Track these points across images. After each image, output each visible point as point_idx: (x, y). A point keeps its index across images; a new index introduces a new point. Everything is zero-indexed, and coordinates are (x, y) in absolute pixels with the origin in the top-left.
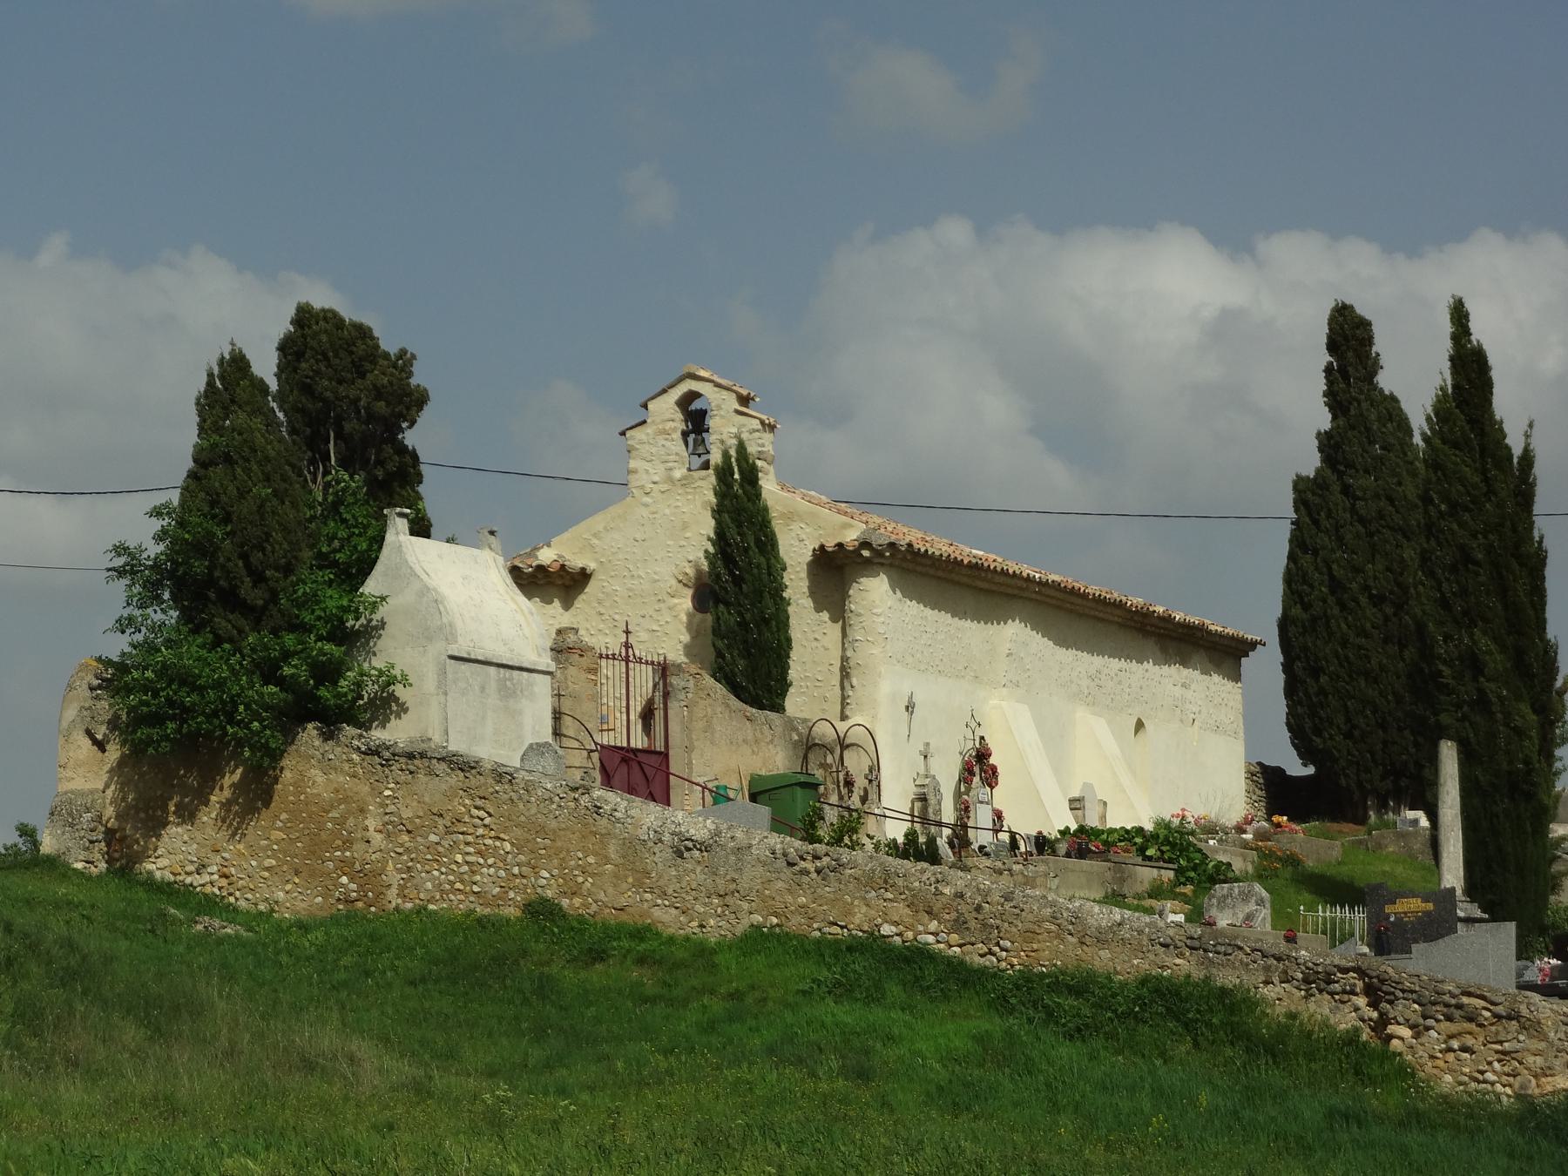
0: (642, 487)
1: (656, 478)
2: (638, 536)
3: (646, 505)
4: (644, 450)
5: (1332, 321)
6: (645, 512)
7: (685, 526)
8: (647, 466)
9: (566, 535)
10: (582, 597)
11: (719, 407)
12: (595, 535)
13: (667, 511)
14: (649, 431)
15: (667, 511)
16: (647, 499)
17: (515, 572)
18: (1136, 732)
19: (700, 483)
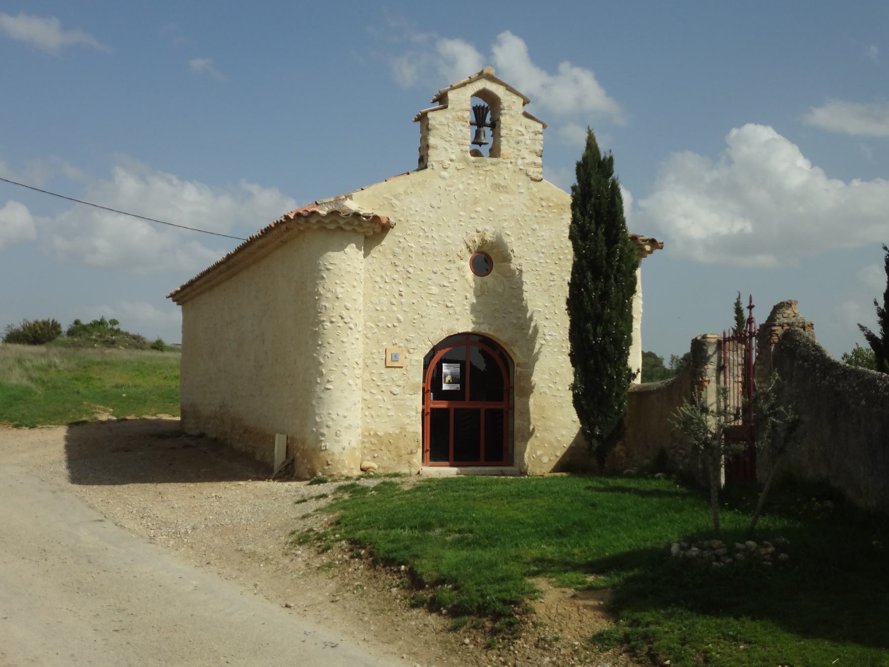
0: (442, 162)
1: (453, 157)
2: (434, 204)
3: (444, 178)
4: (443, 130)
5: (692, 344)
6: (442, 184)
7: (476, 201)
8: (447, 145)
9: (367, 192)
10: (378, 248)
11: (510, 108)
12: (395, 196)
13: (461, 186)
14: (448, 115)
15: (461, 186)
16: (444, 173)
17: (418, 170)
18: (859, 325)
19: (490, 167)
